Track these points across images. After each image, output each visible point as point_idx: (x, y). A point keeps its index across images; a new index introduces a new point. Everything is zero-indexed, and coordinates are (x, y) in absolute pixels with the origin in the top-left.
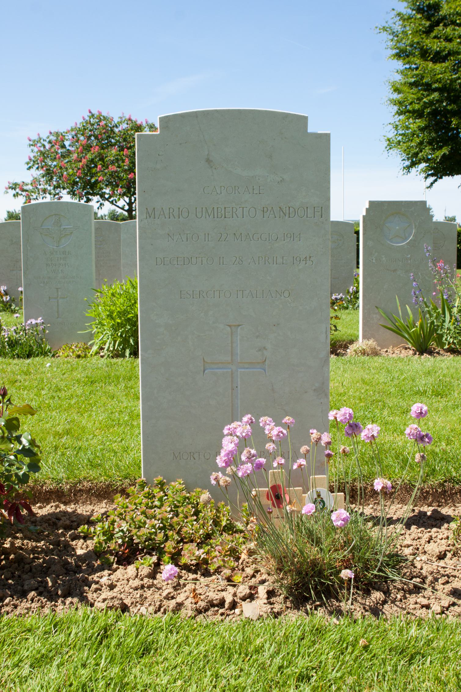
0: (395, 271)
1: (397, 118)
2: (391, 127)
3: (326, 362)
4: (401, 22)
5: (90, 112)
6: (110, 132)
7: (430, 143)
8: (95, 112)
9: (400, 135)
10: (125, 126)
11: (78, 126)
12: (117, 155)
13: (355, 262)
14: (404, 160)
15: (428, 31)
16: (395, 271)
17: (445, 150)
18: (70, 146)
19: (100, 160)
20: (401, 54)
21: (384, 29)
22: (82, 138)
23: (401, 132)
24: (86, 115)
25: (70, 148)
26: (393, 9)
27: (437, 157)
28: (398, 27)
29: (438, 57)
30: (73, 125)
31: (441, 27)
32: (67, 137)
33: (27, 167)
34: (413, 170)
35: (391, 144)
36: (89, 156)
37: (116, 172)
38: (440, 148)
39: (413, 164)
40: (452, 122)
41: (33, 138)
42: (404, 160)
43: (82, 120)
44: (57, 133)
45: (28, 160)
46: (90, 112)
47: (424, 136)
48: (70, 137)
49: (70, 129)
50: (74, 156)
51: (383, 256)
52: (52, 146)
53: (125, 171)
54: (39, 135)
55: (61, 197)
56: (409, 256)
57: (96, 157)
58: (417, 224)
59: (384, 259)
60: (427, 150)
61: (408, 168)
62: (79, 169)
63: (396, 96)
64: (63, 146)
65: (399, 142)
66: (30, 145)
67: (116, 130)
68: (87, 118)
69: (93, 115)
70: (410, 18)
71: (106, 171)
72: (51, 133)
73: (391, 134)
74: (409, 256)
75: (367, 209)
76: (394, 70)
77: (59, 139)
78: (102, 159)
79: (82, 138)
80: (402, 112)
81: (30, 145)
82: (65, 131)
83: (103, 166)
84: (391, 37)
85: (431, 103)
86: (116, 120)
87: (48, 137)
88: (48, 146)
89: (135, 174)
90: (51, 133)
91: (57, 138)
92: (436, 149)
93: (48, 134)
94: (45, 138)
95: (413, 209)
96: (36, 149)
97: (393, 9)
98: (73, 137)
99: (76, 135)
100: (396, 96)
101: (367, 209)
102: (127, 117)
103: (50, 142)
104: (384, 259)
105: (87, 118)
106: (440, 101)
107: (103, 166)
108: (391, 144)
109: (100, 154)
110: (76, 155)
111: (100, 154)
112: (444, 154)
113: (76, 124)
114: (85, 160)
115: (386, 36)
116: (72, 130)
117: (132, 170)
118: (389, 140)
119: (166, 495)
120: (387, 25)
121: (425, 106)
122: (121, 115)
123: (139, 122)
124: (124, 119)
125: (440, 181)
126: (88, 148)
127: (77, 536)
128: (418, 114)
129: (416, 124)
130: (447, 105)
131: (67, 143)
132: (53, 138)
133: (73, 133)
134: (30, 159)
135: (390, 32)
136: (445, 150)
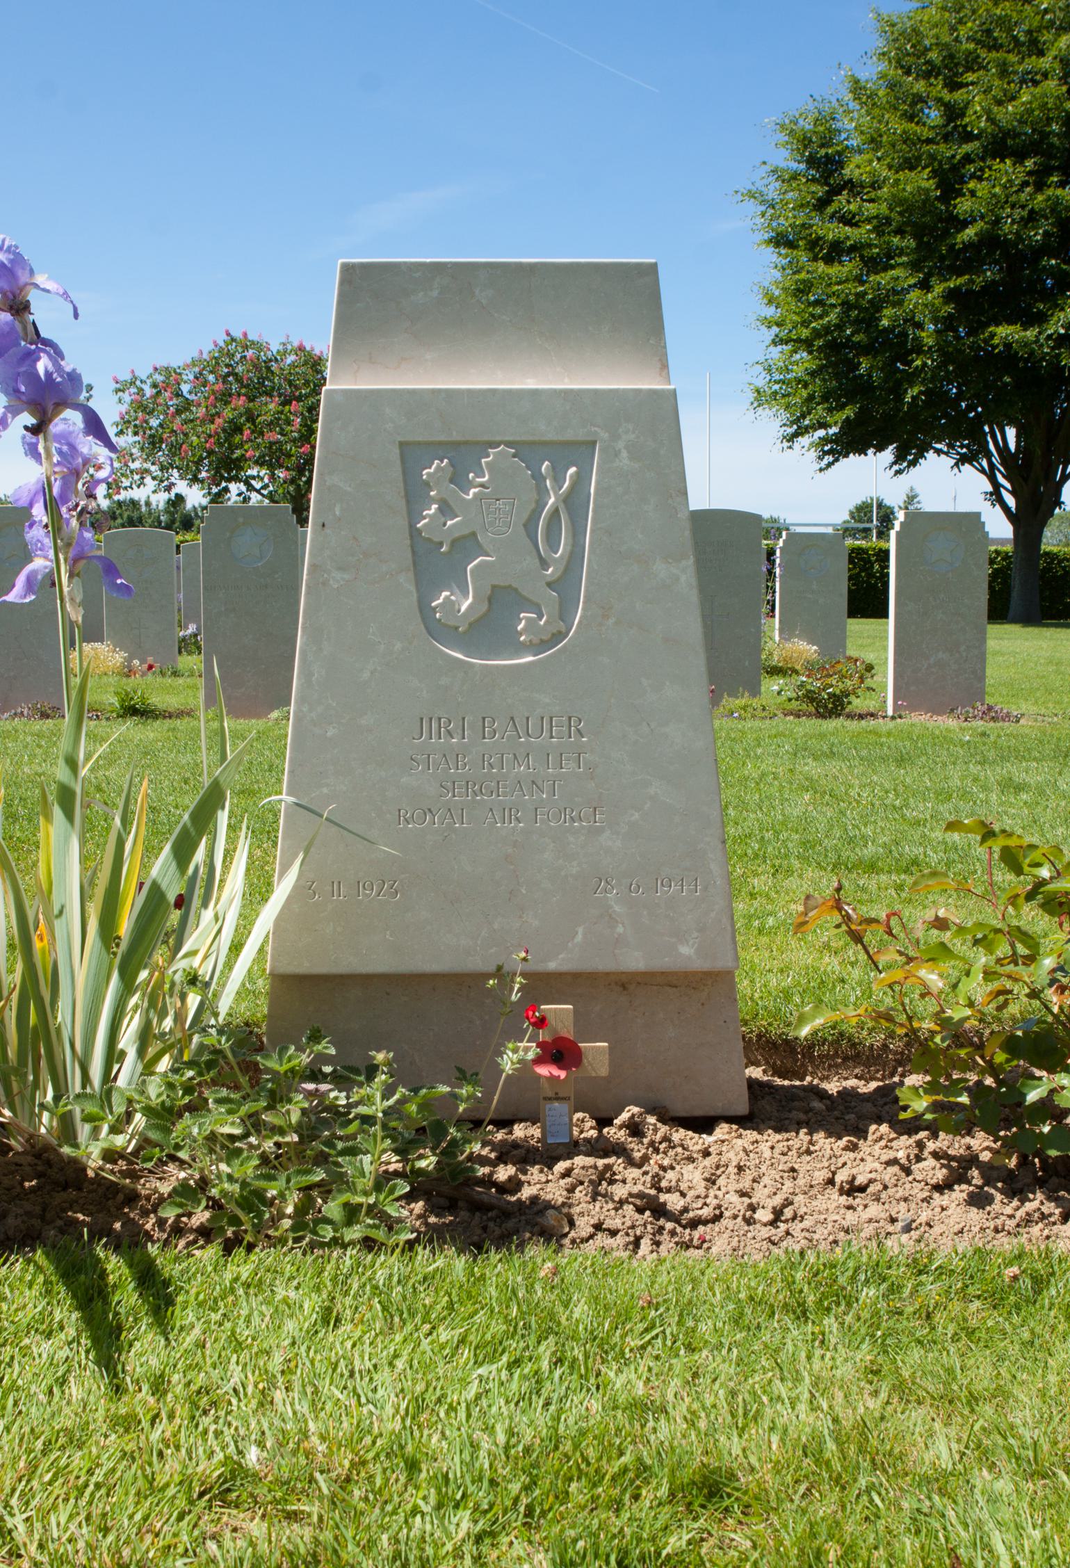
1: (776, 352)
2: (759, 368)
3: (984, 632)
4: (778, 184)
5: (228, 334)
6: (264, 368)
7: (825, 398)
8: (237, 334)
9: (776, 382)
10: (290, 359)
11: (205, 356)
12: (278, 412)
13: (346, 833)
14: (784, 425)
15: (822, 204)
17: (849, 412)
18: (190, 392)
19: (248, 420)
20: (780, 241)
21: (752, 195)
22: (211, 378)
23: (777, 377)
24: (221, 339)
25: (192, 397)
26: (764, 163)
28: (773, 190)
29: (835, 251)
30: (196, 355)
31: (843, 197)
32: (185, 377)
34: (805, 440)
35: (761, 398)
36: (228, 413)
37: (278, 442)
38: (842, 407)
40: (860, 363)
41: (121, 378)
42: (784, 425)
43: (212, 347)
44: (167, 368)
46: (228, 334)
47: (817, 386)
48: (191, 377)
49: (189, 361)
50: (201, 412)
52: (159, 393)
53: (294, 441)
54: (133, 372)
55: (174, 484)
57: (241, 415)
61: (792, 438)
62: (210, 436)
63: (770, 311)
64: (178, 394)
65: (775, 393)
66: (117, 391)
67: (274, 366)
68: (222, 344)
69: (233, 340)
70: (795, 177)
71: (259, 440)
72: (156, 369)
73: (761, 381)
76: (767, 266)
77: (169, 380)
78: (251, 418)
79: (211, 378)
80: (781, 340)
81: (117, 391)
82: (181, 364)
83: (253, 432)
84: (763, 208)
85: (827, 329)
86: (275, 347)
87: (150, 376)
88: (149, 391)
89: (314, 447)
90: (156, 369)
91: (168, 378)
92: (835, 409)
93: (151, 370)
94: (144, 378)
96: (127, 397)
97: (764, 163)
98: (196, 378)
99: (201, 374)
100: (770, 311)
102: (296, 344)
103: (155, 386)
105: (222, 344)
106: (840, 327)
107: (253, 432)
108: (761, 398)
109: (248, 411)
111: (248, 411)
113: (201, 353)
114: (221, 420)
115: (753, 208)
116: (194, 364)
117: (308, 433)
118: (758, 392)
119: (760, 931)
120: (754, 189)
121: (817, 334)
122: (284, 340)
123: (317, 352)
124: (289, 347)
125: (843, 462)
126: (225, 397)
128: (807, 344)
129: (804, 361)
130: (853, 334)
131: (185, 388)
132: (159, 378)
133: (197, 369)
135: (761, 199)
136: (849, 412)
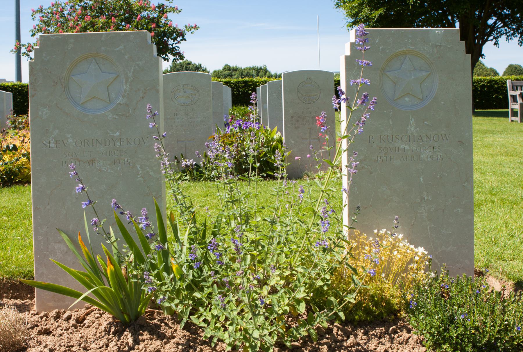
0: (91, 162)
16: (91, 162)
27: (375, 16)
33: (31, 33)
39: (354, 23)
45: (33, 28)
48: (69, 8)
51: (69, 136)
56: (118, 134)
57: (88, 25)
58: (130, 74)
59: (70, 140)
60: (366, 10)
74: (118, 134)
75: (347, 58)
95: (121, 47)
101: (347, 58)
104: (70, 140)
110: (72, 22)
112: (381, 14)
127: (58, 318)
134: (35, 28)
